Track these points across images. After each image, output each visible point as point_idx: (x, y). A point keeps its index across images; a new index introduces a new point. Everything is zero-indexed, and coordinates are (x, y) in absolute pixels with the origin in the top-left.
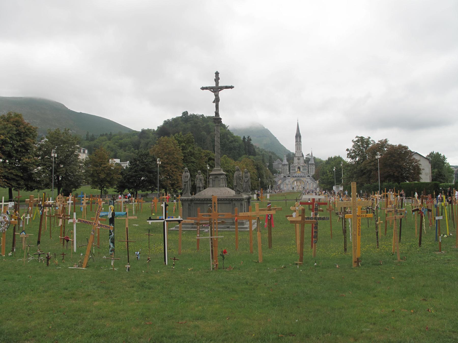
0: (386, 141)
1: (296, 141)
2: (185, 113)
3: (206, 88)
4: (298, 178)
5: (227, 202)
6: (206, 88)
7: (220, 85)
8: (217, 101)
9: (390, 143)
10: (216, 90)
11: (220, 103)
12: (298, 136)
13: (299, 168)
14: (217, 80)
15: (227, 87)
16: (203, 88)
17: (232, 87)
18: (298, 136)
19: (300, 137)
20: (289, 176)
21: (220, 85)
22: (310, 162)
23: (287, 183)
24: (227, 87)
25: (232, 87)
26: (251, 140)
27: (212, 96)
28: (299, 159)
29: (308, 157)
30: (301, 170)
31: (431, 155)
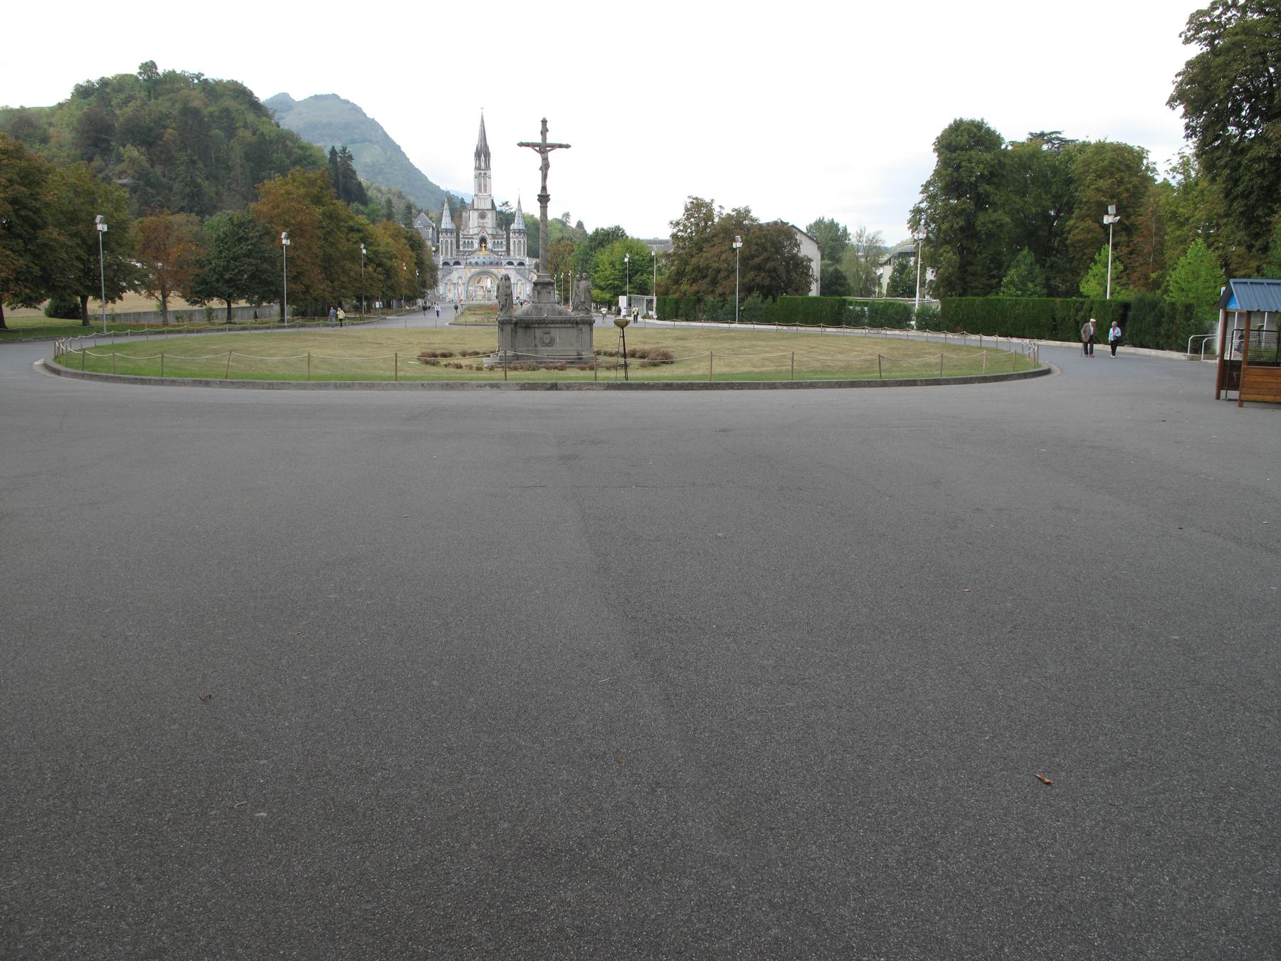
0: (748, 211)
1: (478, 168)
2: (149, 67)
3: (527, 145)
4: (486, 268)
5: (472, 319)
6: (527, 145)
7: (548, 141)
8: (545, 167)
9: (753, 214)
10: (543, 148)
11: (550, 172)
12: (483, 153)
13: (483, 240)
14: (544, 131)
15: (561, 146)
16: (521, 145)
17: (567, 146)
18: (483, 153)
19: (487, 155)
20: (457, 263)
21: (548, 141)
22: (512, 227)
23: (455, 281)
24: (561, 146)
25: (567, 146)
26: (350, 157)
27: (537, 159)
28: (482, 216)
29: (504, 209)
30: (490, 246)
31: (819, 224)
